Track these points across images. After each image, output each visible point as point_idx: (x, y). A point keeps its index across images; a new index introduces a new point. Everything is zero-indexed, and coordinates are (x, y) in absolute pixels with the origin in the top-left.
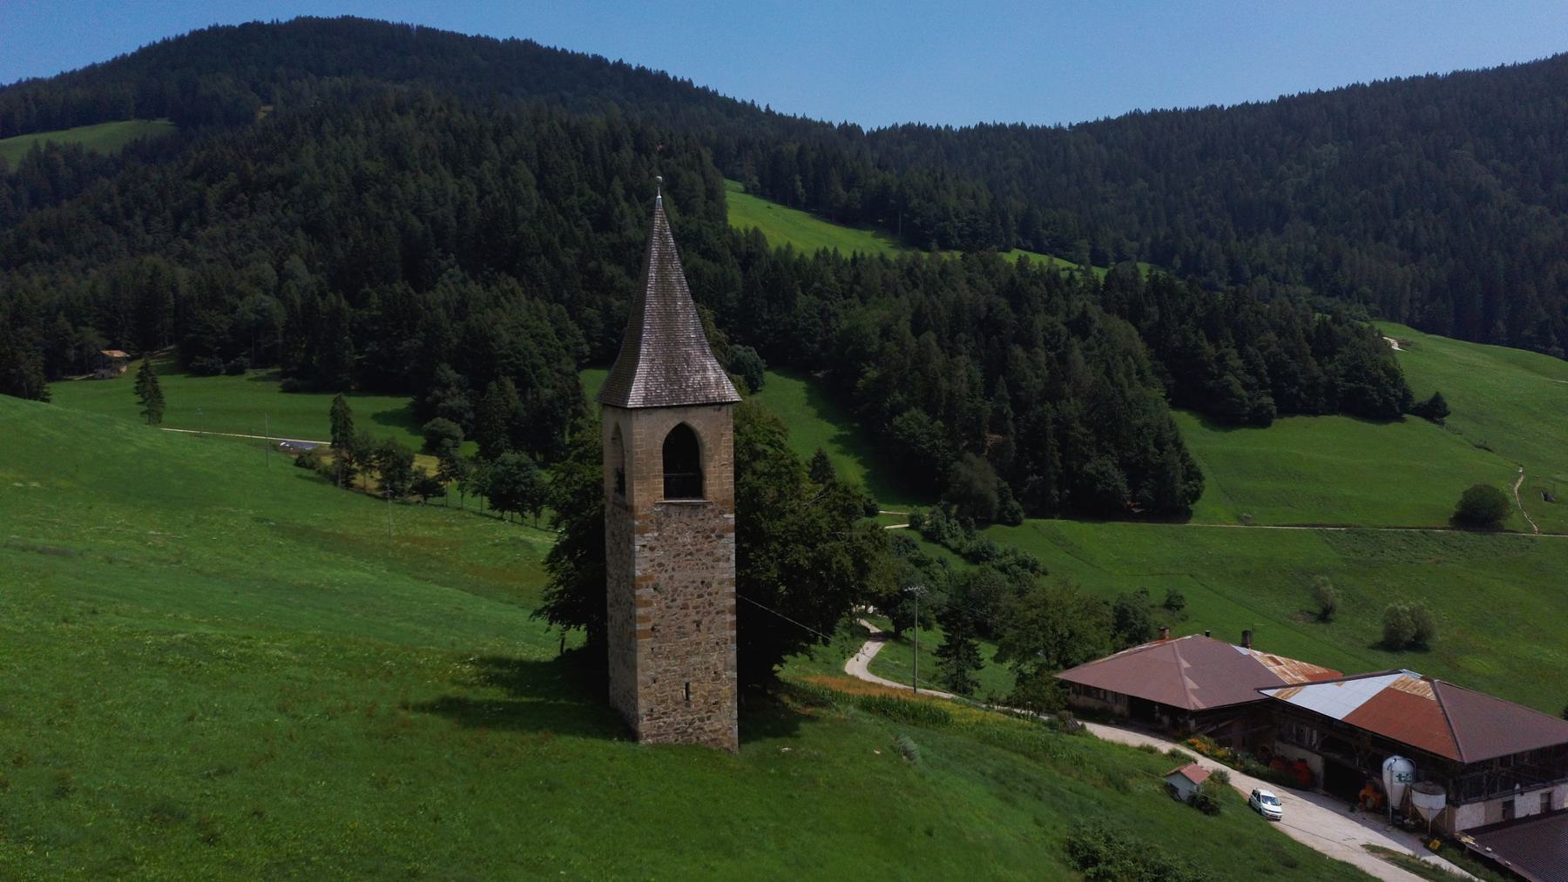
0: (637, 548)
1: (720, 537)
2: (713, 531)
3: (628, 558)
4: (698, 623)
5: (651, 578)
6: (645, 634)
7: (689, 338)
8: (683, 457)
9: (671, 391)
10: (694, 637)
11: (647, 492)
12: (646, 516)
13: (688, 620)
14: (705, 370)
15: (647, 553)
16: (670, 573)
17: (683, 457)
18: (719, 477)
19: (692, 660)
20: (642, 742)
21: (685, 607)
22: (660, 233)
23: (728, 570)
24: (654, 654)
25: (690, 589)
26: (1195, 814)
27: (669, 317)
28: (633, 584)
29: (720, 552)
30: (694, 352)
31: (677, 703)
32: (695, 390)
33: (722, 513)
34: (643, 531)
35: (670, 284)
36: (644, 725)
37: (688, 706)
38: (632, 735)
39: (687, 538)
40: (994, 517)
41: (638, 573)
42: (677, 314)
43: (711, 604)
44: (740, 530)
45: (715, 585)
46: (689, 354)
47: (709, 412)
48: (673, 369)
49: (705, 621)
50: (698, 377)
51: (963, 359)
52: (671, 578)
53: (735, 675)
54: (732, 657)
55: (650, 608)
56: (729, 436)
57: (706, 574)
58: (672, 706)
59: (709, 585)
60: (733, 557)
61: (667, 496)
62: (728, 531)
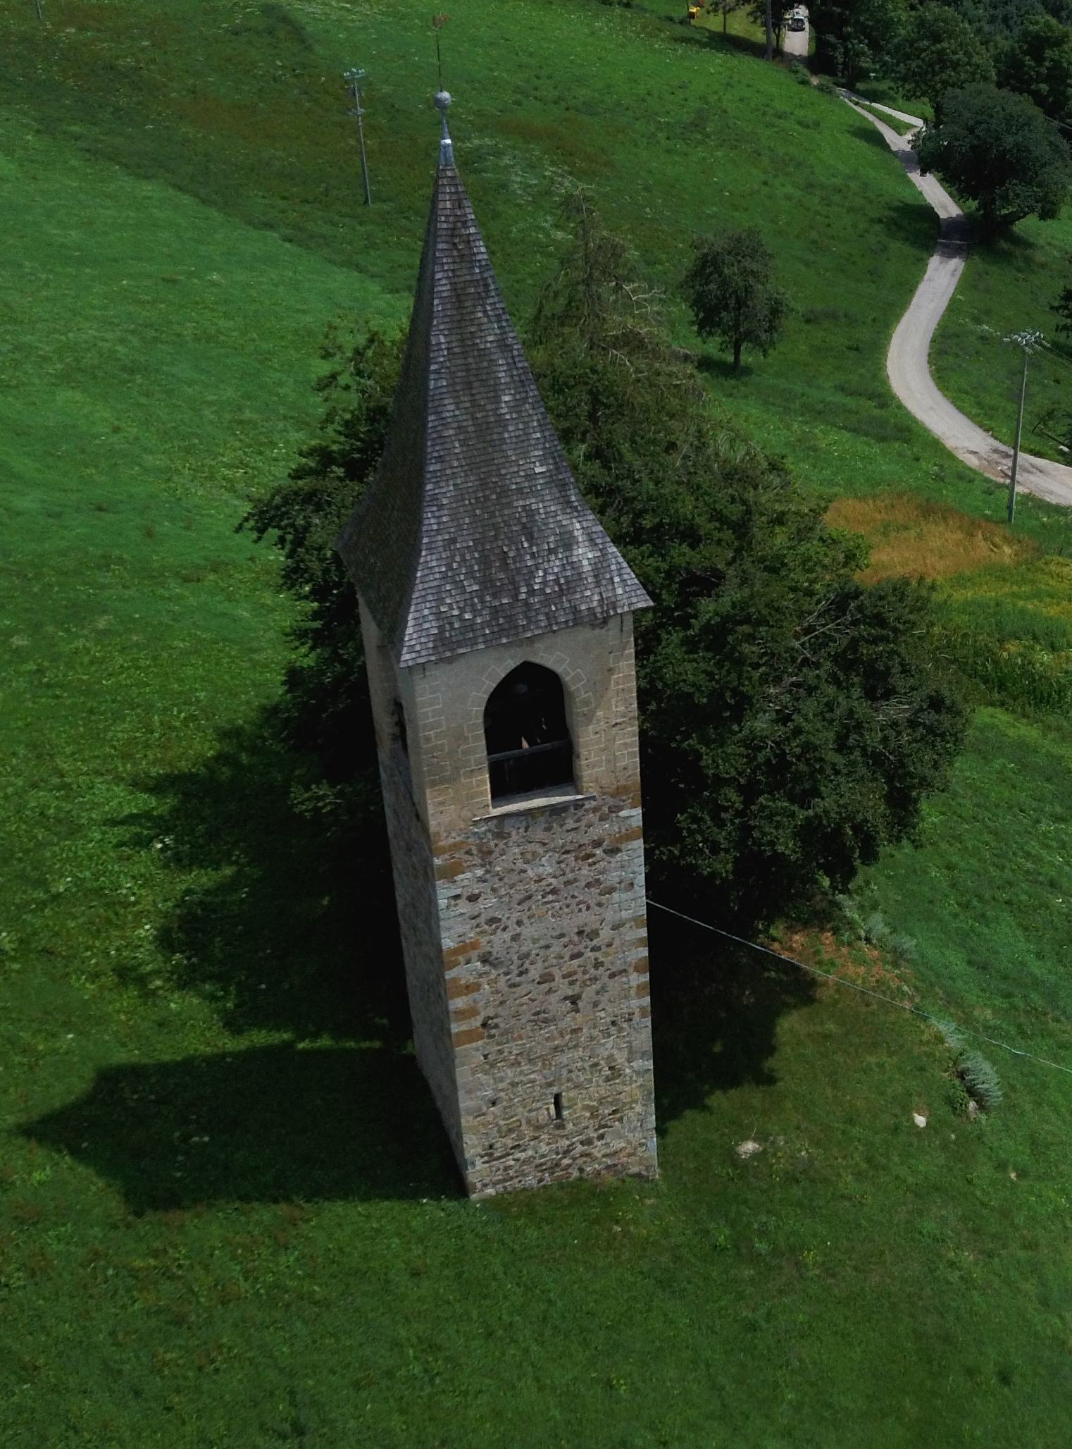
0: (442, 903)
1: (613, 851)
2: (598, 844)
3: (430, 916)
4: (574, 1000)
5: (474, 946)
6: (470, 1036)
7: (531, 476)
8: (529, 734)
9: (495, 611)
10: (568, 1022)
11: (456, 802)
12: (456, 847)
13: (554, 998)
14: (568, 543)
15: (464, 907)
16: (514, 929)
17: (529, 734)
18: (608, 741)
19: (563, 1058)
20: (474, 1197)
21: (547, 978)
22: (453, 233)
23: (635, 902)
24: (490, 1064)
25: (557, 948)
26: (862, 145)
27: (485, 437)
28: (438, 960)
29: (613, 877)
30: (545, 506)
31: (538, 1128)
32: (547, 601)
33: (615, 809)
34: (450, 873)
35: (483, 354)
36: (477, 1171)
37: (561, 1126)
38: (450, 1179)
39: (547, 866)
40: (1008, 481)
41: (448, 943)
42: (501, 422)
43: (598, 964)
44: (649, 830)
45: (606, 933)
46: (531, 513)
47: (586, 634)
48: (497, 565)
49: (589, 993)
50: (555, 565)
51: (841, 60)
52: (515, 938)
53: (650, 1064)
54: (643, 1037)
55: (471, 992)
56: (625, 673)
57: (588, 919)
58: (528, 1132)
59: (595, 934)
60: (641, 879)
61: (500, 792)
62: (629, 837)
